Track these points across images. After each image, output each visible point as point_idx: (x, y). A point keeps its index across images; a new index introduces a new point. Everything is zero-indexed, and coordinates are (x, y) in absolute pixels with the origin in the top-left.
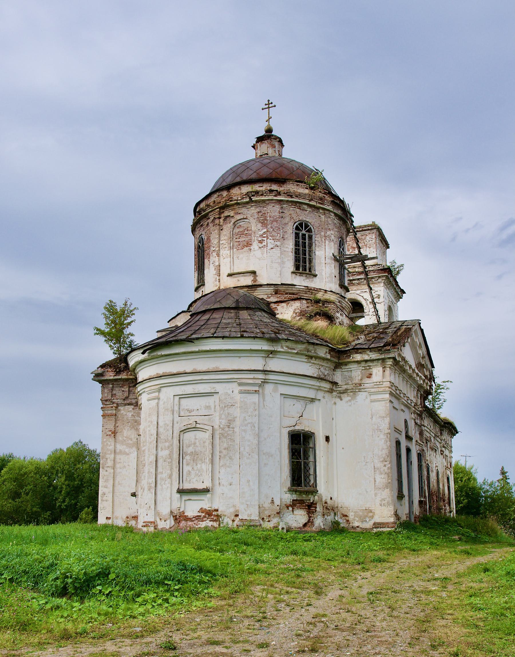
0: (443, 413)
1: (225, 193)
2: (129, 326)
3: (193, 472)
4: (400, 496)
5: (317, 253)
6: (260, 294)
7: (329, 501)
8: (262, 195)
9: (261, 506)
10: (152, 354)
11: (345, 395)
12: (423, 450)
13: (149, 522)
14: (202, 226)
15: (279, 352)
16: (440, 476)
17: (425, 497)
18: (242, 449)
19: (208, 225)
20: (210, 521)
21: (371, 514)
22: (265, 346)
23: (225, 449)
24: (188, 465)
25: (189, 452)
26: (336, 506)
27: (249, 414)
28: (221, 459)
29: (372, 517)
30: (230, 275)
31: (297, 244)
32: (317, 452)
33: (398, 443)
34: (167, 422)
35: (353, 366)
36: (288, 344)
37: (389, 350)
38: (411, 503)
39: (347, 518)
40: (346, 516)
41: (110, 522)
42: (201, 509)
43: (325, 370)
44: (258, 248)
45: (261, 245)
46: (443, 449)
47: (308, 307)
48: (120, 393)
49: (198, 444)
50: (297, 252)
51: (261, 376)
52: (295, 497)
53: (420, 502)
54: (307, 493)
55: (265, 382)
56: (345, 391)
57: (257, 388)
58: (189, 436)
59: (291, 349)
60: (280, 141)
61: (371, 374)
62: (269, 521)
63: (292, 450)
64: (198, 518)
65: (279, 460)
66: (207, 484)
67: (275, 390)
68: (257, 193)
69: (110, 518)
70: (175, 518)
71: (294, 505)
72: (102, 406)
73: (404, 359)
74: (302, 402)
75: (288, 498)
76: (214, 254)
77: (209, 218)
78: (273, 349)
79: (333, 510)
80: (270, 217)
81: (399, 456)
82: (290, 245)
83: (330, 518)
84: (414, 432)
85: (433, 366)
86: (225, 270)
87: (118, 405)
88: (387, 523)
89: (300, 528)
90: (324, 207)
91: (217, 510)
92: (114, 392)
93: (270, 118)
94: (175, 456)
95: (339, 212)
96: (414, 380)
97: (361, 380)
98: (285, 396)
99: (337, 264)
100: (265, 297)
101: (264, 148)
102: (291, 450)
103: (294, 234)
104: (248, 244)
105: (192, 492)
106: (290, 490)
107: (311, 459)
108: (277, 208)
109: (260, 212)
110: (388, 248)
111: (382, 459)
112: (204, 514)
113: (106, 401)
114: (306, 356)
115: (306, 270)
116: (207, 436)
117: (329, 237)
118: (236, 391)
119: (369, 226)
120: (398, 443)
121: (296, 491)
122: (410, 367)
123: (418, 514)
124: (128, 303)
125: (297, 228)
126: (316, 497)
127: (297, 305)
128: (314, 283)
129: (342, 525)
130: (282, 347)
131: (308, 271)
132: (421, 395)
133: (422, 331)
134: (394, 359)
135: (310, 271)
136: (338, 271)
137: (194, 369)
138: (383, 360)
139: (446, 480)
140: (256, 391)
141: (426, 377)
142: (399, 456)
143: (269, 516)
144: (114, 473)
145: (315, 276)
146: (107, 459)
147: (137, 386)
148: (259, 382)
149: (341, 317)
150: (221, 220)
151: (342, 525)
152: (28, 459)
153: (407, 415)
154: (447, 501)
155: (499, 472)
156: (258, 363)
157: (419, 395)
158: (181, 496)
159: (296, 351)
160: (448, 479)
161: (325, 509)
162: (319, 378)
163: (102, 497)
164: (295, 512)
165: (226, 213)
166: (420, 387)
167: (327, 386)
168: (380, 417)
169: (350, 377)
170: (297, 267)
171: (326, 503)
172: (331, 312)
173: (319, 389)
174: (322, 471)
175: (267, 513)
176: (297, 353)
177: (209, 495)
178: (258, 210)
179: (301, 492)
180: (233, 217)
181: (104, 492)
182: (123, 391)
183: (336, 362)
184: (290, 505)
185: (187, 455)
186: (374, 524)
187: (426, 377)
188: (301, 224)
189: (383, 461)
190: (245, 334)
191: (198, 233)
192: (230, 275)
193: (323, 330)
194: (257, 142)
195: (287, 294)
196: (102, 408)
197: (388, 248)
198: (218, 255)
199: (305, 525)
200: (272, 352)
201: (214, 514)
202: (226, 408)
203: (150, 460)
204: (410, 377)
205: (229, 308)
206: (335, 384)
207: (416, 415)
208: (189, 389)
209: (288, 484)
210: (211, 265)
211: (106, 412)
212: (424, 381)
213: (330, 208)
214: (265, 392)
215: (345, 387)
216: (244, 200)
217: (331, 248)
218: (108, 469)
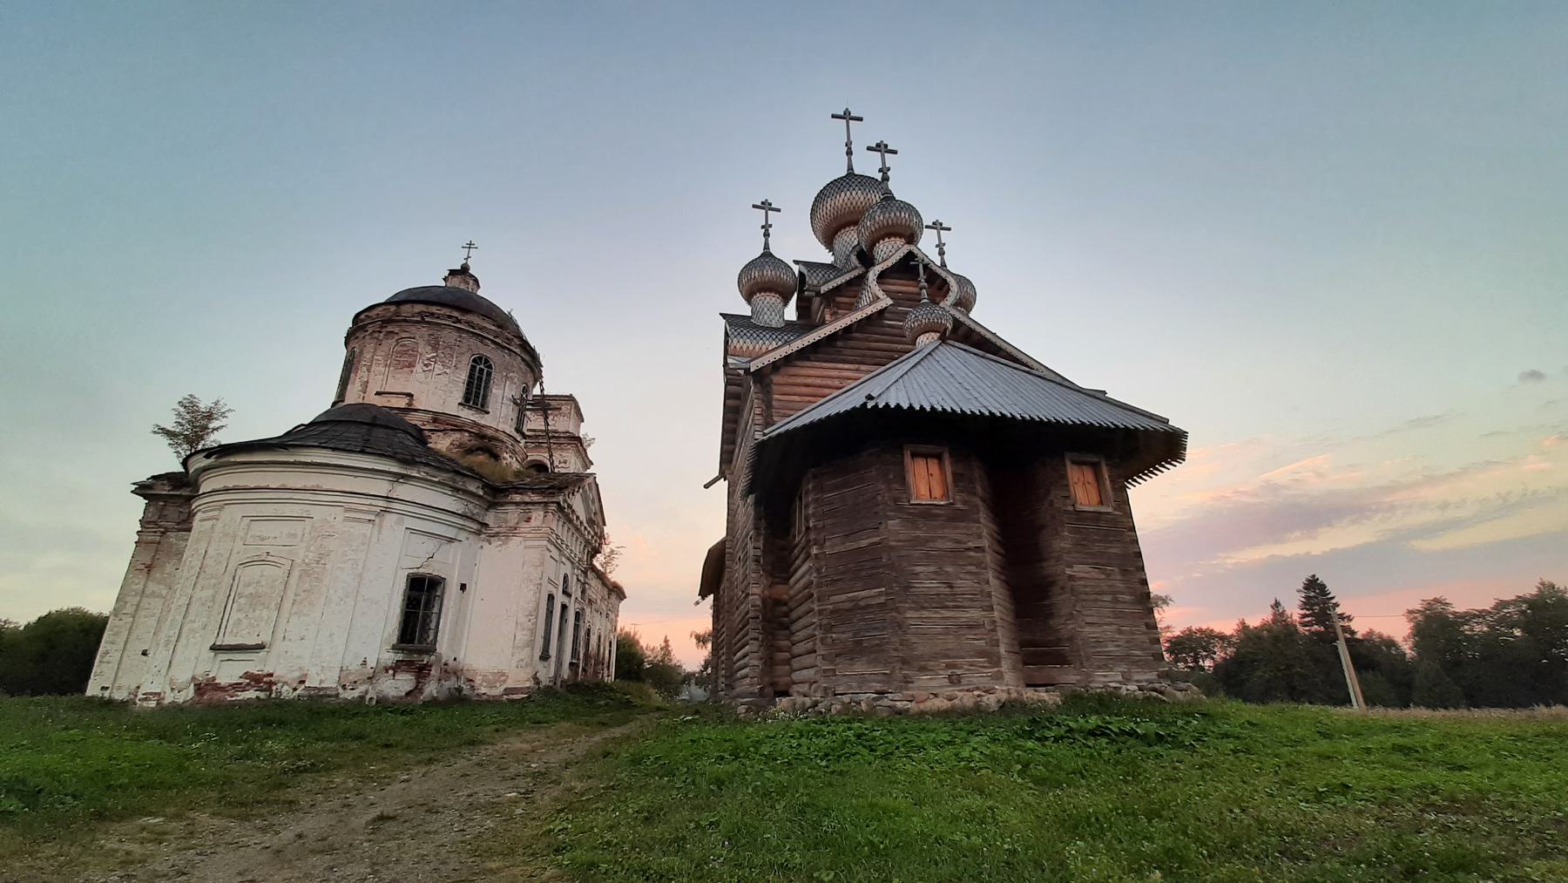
0: (614, 577)
1: (393, 308)
2: (215, 432)
3: (245, 622)
4: (545, 657)
5: (494, 390)
6: (414, 419)
7: (451, 662)
8: (438, 318)
9: (344, 668)
10: (221, 460)
11: (496, 538)
12: (584, 609)
13: (151, 694)
14: (357, 338)
15: (415, 477)
16: (602, 640)
17: (579, 659)
18: (331, 591)
19: (364, 337)
20: (256, 690)
21: (503, 678)
22: (394, 468)
23: (304, 591)
24: (239, 611)
25: (247, 593)
26: (461, 668)
27: (354, 548)
28: (296, 603)
29: (505, 681)
30: (378, 393)
31: (471, 376)
32: (445, 602)
33: (551, 597)
34: (222, 552)
35: (511, 508)
36: (427, 469)
37: (554, 493)
38: (559, 663)
39: (472, 684)
40: (472, 681)
41: (107, 694)
42: (246, 673)
43: (474, 510)
44: (421, 370)
45: (426, 369)
46: (609, 612)
47: (469, 441)
48: (173, 512)
49: (263, 583)
50: (470, 384)
51: (382, 503)
52: (400, 657)
53: (571, 664)
54: (420, 652)
55: (386, 511)
56: (496, 535)
57: (372, 518)
58: (255, 571)
59: (431, 476)
60: (476, 281)
61: (530, 518)
62: (352, 689)
63: (409, 598)
64: (236, 687)
65: (387, 609)
66: (265, 638)
67: (399, 522)
68: (432, 314)
69: (107, 688)
70: (197, 687)
71: (397, 667)
72: (140, 529)
73: (570, 506)
74: (436, 541)
75: (390, 657)
76: (365, 369)
77: (367, 331)
78: (405, 473)
79: (455, 673)
80: (443, 342)
81: (550, 613)
82: (464, 376)
83: (451, 683)
84: (575, 589)
85: (605, 525)
86: (374, 387)
87: (167, 530)
88: (522, 688)
89: (401, 698)
90: (511, 348)
91: (271, 675)
92: (165, 512)
93: (469, 257)
94: (221, 598)
95: (527, 358)
96: (582, 535)
97: (517, 523)
98: (413, 531)
99: (517, 408)
100: (419, 423)
101: (456, 282)
102: (406, 598)
103: (469, 367)
104: (411, 365)
105: (235, 649)
106: (394, 648)
107: (436, 610)
108: (455, 334)
109: (432, 335)
110: (583, 421)
111: (528, 613)
112: (248, 681)
113: (149, 523)
114: (451, 487)
115: (477, 405)
116: (280, 573)
117: (511, 378)
118: (340, 518)
119: (566, 396)
120: (551, 597)
121: (403, 650)
122: (578, 518)
123: (566, 677)
124: (221, 403)
125: (474, 361)
126: (433, 657)
127: (457, 435)
128: (483, 420)
129: (464, 692)
130: (419, 472)
131: (479, 406)
132: (588, 551)
133: (597, 485)
134: (558, 503)
135: (482, 406)
136: (516, 416)
137: (283, 485)
138: (546, 504)
139: (607, 644)
140: (370, 520)
141: (596, 534)
142: (550, 613)
143: (355, 682)
144: (133, 623)
145: (488, 413)
146: (126, 602)
147: (192, 501)
148: (378, 509)
149: (509, 459)
150: (382, 335)
151: (464, 692)
152: (90, 612)
153: (567, 568)
154: (605, 665)
155: (663, 640)
156: (381, 487)
157: (586, 551)
158: (215, 655)
159: (437, 480)
160: (610, 643)
161: (443, 673)
162: (462, 516)
163: (102, 657)
164: (397, 677)
165: (390, 328)
166: (588, 542)
167: (475, 526)
168: (532, 565)
169: (506, 521)
170: (467, 399)
171: (446, 664)
172: (497, 451)
173: (463, 528)
174: (448, 628)
175: (352, 678)
176: (438, 483)
177: (262, 653)
178: (430, 332)
179: (411, 652)
180: (397, 333)
181: (107, 650)
182: (180, 512)
183: (489, 501)
184: (391, 668)
185: (242, 597)
186: (505, 689)
187: (596, 534)
188: (480, 358)
189: (527, 615)
190: (368, 450)
191: (354, 344)
192: (378, 393)
193: (481, 464)
194: (449, 275)
195: (447, 424)
196: (139, 532)
197: (583, 421)
198: (369, 371)
199: (408, 694)
200: (403, 476)
201: (265, 679)
202: (319, 539)
203: (180, 603)
204: (577, 529)
205: (361, 423)
206: (486, 525)
207: (579, 571)
208: (268, 510)
209: (394, 640)
210: (358, 380)
211: (144, 538)
212: (592, 537)
213: (517, 351)
214: (385, 524)
215: (497, 530)
216: (415, 319)
217: (511, 390)
218: (124, 617)
